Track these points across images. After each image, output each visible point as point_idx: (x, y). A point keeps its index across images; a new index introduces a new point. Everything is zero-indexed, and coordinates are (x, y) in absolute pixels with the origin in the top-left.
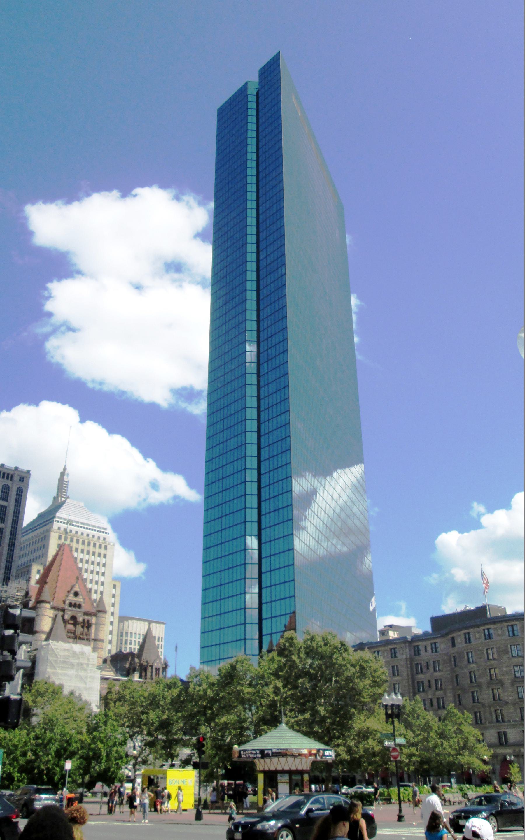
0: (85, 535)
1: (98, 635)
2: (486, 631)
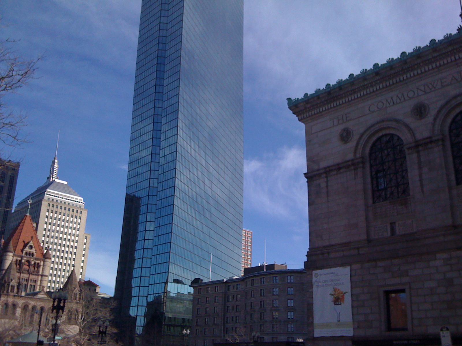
1: (44, 272)
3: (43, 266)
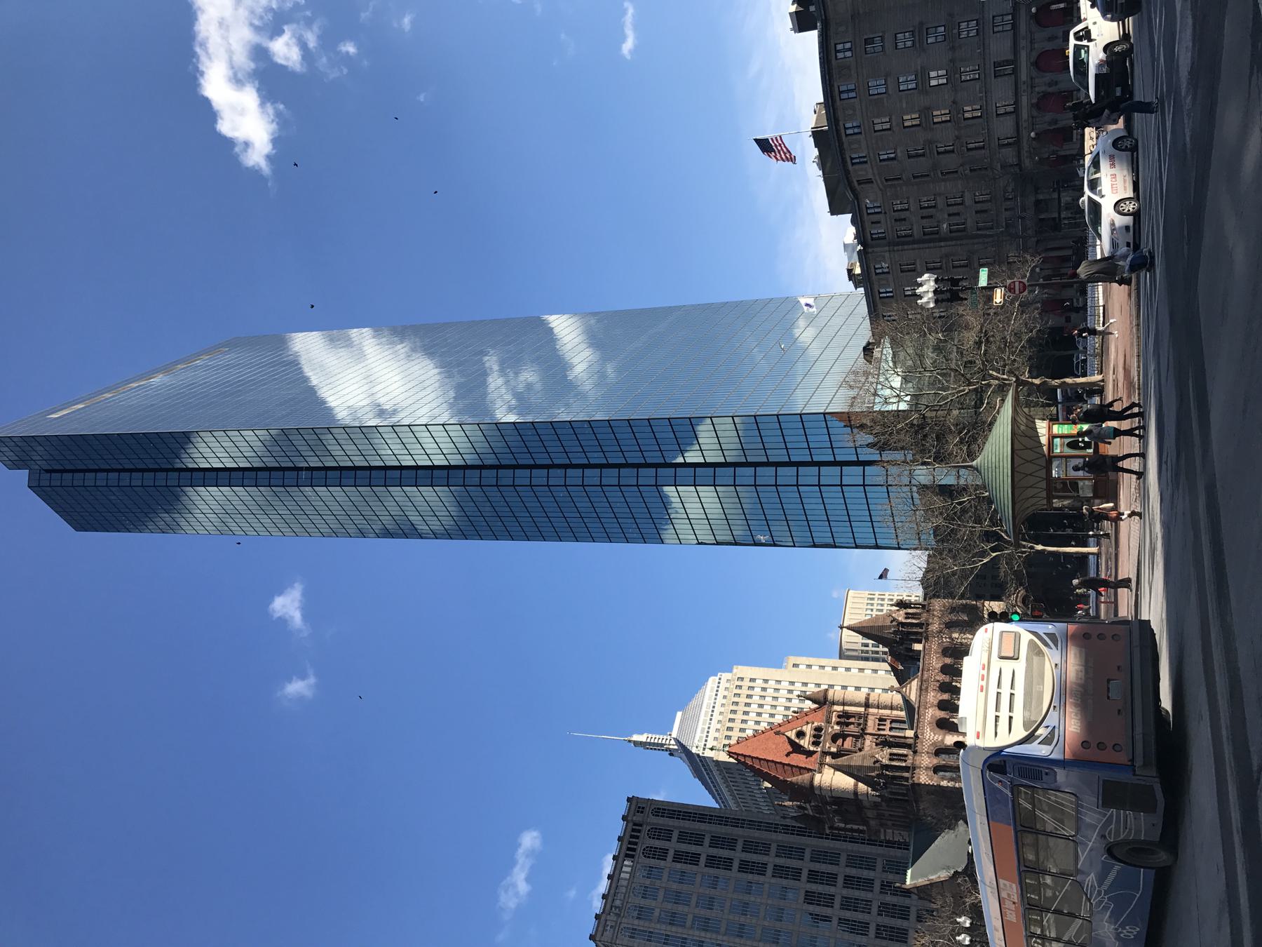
0: (722, 709)
3: (844, 704)
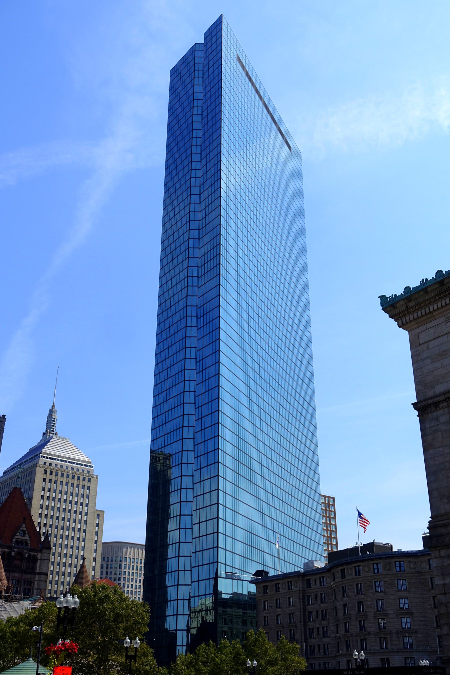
2: (357, 568)
